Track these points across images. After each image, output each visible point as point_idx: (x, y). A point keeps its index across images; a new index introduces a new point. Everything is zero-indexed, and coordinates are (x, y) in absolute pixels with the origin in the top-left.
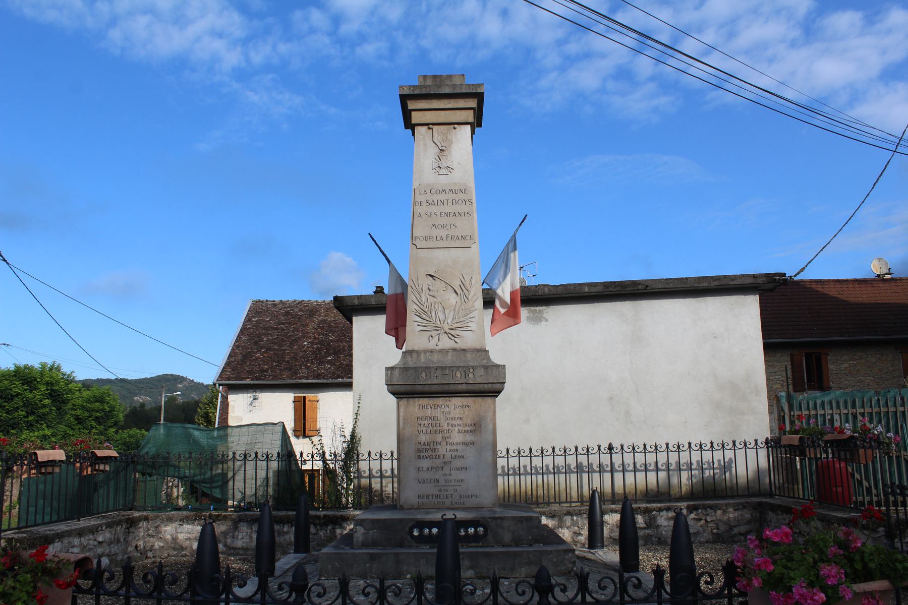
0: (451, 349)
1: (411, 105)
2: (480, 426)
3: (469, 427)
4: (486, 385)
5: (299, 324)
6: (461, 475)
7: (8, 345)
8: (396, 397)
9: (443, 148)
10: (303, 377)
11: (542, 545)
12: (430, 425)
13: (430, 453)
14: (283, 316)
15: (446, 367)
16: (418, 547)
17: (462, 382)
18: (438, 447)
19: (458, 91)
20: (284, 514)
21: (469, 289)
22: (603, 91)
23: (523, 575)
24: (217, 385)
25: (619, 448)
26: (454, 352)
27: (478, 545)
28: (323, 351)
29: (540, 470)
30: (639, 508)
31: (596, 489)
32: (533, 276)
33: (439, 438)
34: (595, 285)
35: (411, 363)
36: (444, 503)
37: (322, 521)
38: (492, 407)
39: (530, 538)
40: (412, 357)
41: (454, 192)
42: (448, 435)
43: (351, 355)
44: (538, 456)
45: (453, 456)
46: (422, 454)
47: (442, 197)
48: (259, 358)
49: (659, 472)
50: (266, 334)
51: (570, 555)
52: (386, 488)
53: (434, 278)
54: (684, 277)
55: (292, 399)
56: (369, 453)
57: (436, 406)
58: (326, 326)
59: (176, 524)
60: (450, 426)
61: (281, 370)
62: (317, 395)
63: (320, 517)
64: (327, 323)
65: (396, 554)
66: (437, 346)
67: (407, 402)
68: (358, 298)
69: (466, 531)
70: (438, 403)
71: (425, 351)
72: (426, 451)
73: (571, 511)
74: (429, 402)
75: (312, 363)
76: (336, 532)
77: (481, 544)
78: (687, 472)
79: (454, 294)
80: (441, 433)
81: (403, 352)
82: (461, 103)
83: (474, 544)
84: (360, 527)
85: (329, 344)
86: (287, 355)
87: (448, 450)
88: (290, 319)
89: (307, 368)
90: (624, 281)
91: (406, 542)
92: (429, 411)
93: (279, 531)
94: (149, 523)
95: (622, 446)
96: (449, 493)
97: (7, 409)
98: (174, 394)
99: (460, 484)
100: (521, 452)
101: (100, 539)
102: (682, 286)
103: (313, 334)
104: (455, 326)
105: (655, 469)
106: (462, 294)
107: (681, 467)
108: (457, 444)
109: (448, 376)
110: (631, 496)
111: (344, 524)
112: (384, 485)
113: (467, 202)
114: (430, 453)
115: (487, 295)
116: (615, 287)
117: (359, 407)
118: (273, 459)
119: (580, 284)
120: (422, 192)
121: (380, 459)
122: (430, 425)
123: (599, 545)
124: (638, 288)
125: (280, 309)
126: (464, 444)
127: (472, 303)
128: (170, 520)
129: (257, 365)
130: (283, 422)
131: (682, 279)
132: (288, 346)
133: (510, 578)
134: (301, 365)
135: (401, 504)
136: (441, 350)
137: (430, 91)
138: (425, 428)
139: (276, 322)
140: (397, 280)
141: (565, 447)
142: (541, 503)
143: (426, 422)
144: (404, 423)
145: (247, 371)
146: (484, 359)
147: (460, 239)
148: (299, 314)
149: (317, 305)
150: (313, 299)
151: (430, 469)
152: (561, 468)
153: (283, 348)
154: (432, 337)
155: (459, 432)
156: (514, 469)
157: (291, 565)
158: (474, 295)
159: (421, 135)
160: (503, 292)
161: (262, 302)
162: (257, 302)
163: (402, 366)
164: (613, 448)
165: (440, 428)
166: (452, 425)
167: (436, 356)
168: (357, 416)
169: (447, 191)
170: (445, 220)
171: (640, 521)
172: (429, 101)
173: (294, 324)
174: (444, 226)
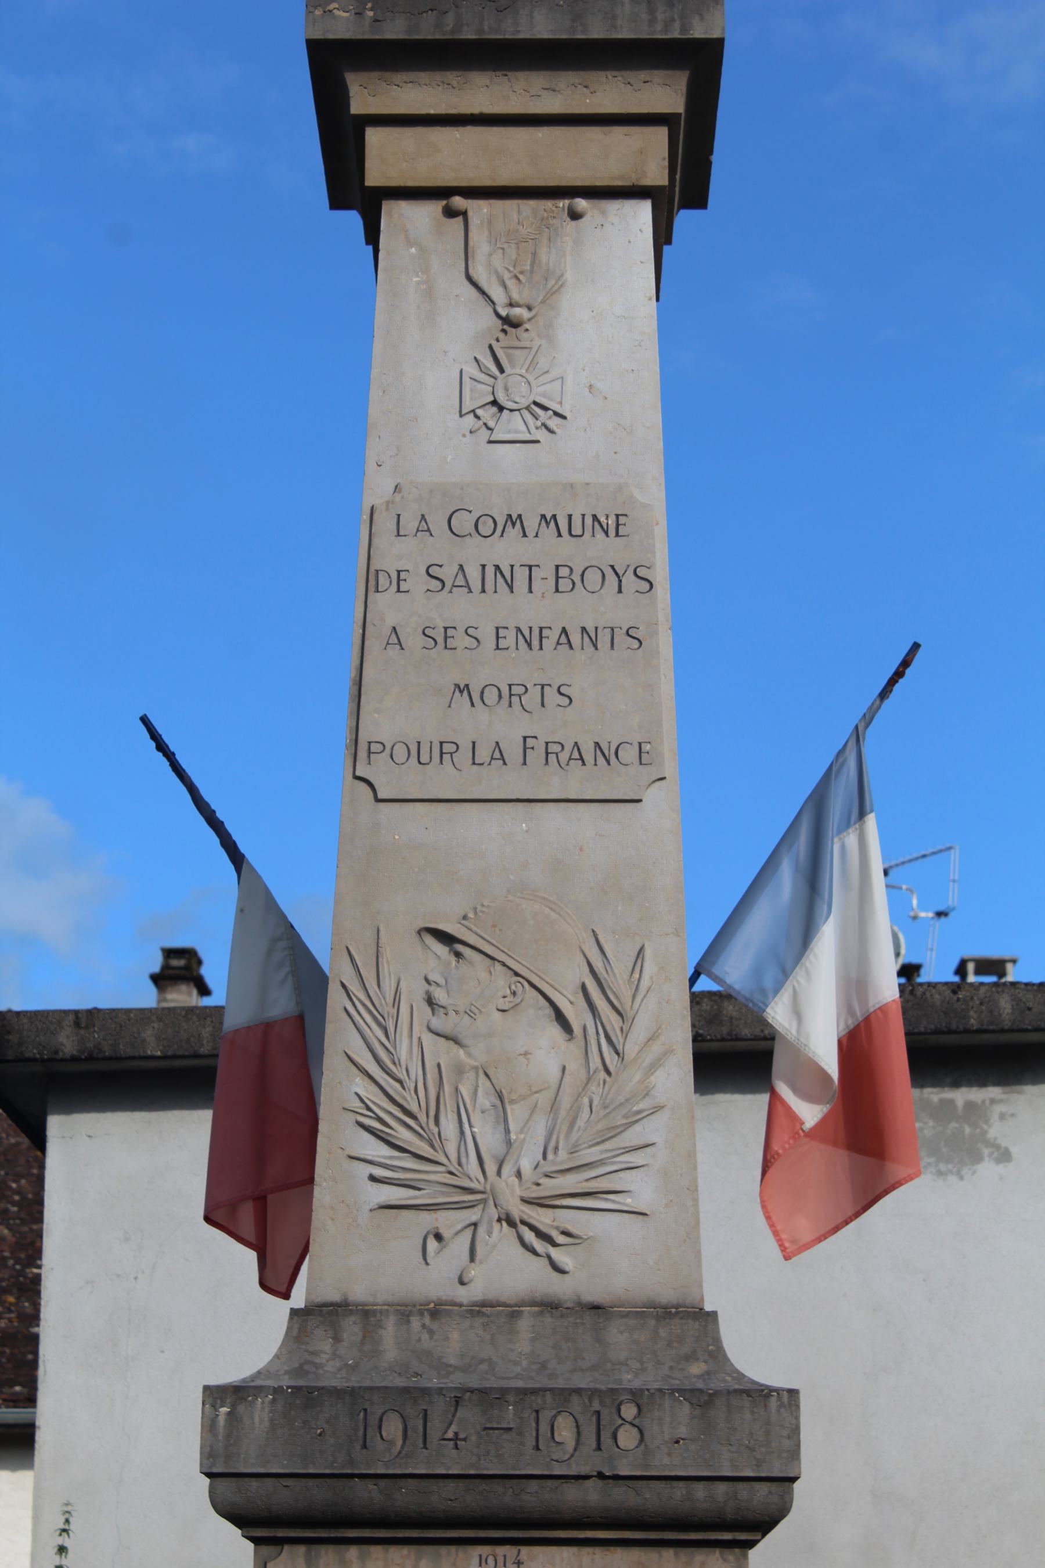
0: (533, 1303)
4: (700, 1490)
17: (584, 1470)
21: (626, 1005)
32: (940, 914)
35: (331, 1366)
40: (337, 1339)
43: (32, 1288)
53: (460, 948)
66: (462, 1283)
68: (77, 1024)
79: (555, 1031)
81: (294, 1312)
113: (629, 579)
120: (410, 524)
127: (638, 1077)
136: (484, 1304)
147: (589, 757)
154: (438, 1237)
160: (797, 1013)
163: (286, 1382)
167: (455, 1336)
172: (452, 77)
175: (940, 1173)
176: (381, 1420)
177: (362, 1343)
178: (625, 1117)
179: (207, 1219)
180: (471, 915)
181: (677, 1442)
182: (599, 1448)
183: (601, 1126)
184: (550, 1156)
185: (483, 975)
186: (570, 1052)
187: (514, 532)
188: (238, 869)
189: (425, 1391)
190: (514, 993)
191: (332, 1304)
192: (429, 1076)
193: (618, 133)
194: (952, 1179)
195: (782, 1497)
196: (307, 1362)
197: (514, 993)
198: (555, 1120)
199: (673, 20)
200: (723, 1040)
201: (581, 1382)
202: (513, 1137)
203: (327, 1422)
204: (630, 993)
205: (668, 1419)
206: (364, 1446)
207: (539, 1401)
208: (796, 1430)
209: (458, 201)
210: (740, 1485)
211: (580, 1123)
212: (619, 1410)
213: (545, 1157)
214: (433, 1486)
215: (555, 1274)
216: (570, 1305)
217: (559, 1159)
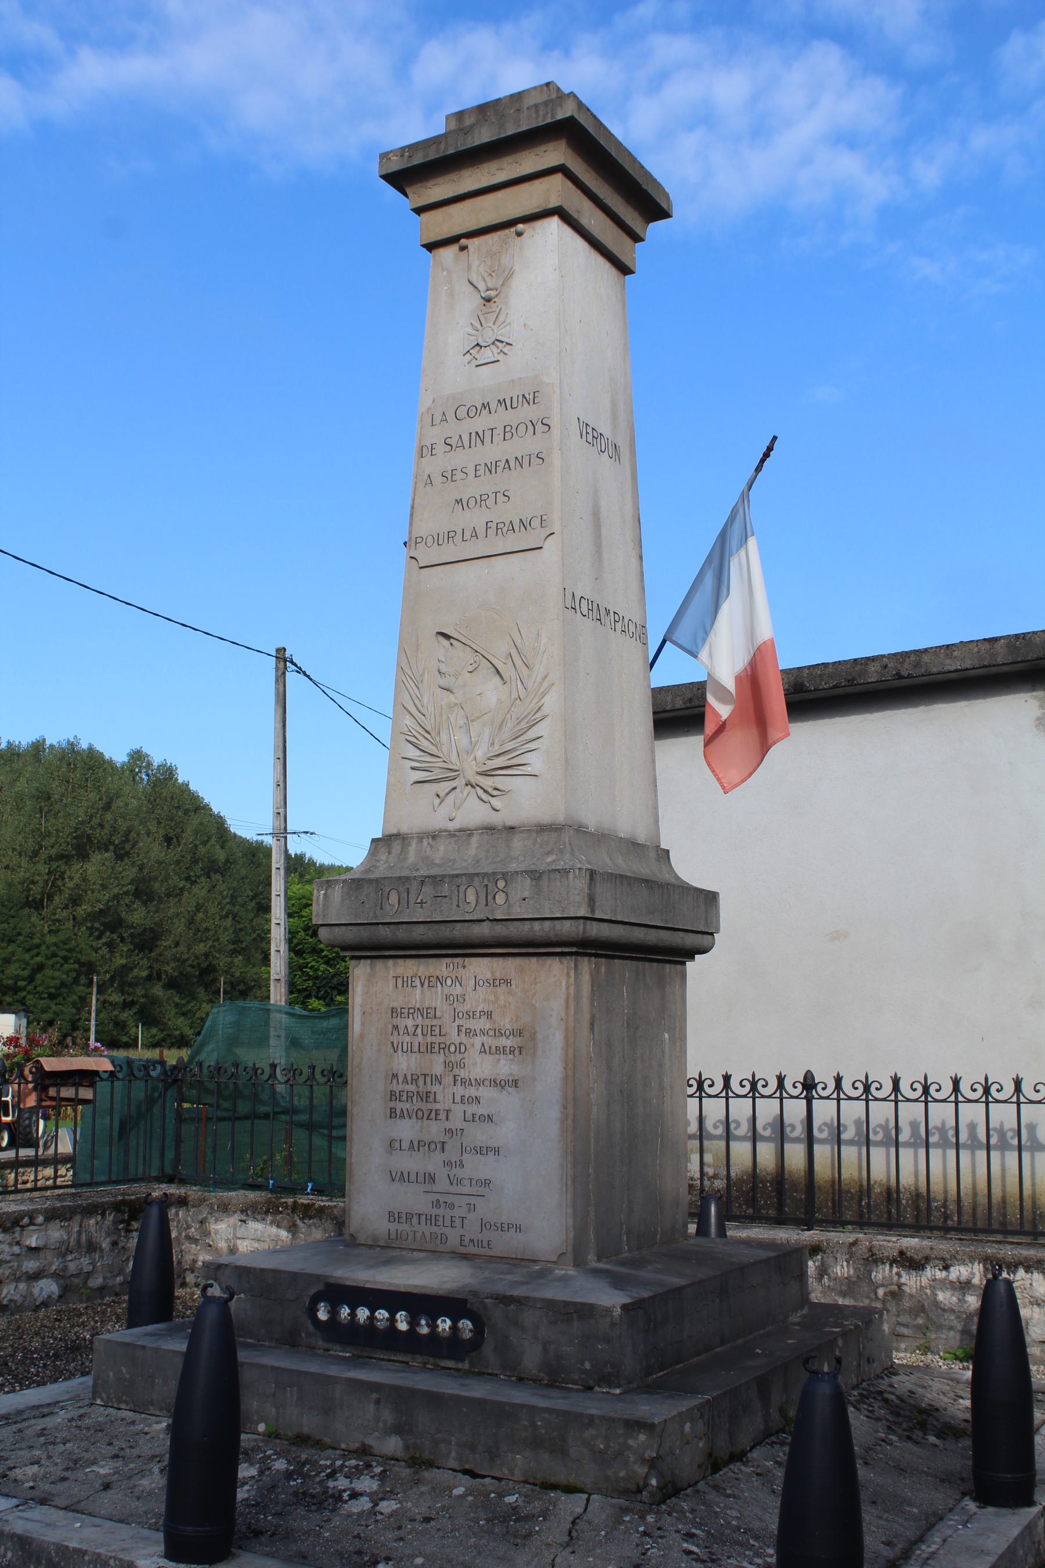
2: (533, 1036)
3: (507, 1038)
4: (537, 925)
7: (312, 834)
12: (419, 1031)
13: (418, 1104)
15: (443, 876)
16: (328, 1350)
27: (460, 1366)
29: (1012, 1138)
36: (444, 1239)
40: (390, 853)
42: (459, 1057)
45: (469, 1116)
46: (399, 1106)
47: (481, 423)
51: (642, 1437)
53: (452, 641)
59: (234, 1219)
67: (372, 968)
69: (433, 1326)
70: (439, 973)
71: (421, 837)
74: (418, 970)
79: (497, 679)
80: (442, 1051)
82: (529, 161)
83: (450, 1364)
87: (458, 1099)
91: (303, 1335)
94: (189, 1211)
96: (457, 1213)
97: (326, 956)
101: (33, 1242)
108: (479, 1083)
109: (447, 899)
113: (539, 427)
115: (915, 666)
120: (438, 418)
122: (419, 1031)
126: (495, 1083)
128: (225, 1208)
133: (483, 1477)
137: (446, 149)
138: (407, 1039)
143: (410, 1023)
144: (363, 1024)
147: (516, 528)
159: (443, 270)
166: (468, 1032)
167: (442, 848)
170: (486, 485)
172: (453, 176)
174: (481, 500)
181: (524, 900)
182: (487, 905)
187: (485, 412)
189: (408, 878)
193: (537, 183)
199: (547, 113)
200: (923, 675)
203: (366, 896)
205: (520, 888)
206: (381, 908)
209: (463, 242)
210: (557, 922)
212: (496, 884)
214: (414, 927)
216: (500, 828)
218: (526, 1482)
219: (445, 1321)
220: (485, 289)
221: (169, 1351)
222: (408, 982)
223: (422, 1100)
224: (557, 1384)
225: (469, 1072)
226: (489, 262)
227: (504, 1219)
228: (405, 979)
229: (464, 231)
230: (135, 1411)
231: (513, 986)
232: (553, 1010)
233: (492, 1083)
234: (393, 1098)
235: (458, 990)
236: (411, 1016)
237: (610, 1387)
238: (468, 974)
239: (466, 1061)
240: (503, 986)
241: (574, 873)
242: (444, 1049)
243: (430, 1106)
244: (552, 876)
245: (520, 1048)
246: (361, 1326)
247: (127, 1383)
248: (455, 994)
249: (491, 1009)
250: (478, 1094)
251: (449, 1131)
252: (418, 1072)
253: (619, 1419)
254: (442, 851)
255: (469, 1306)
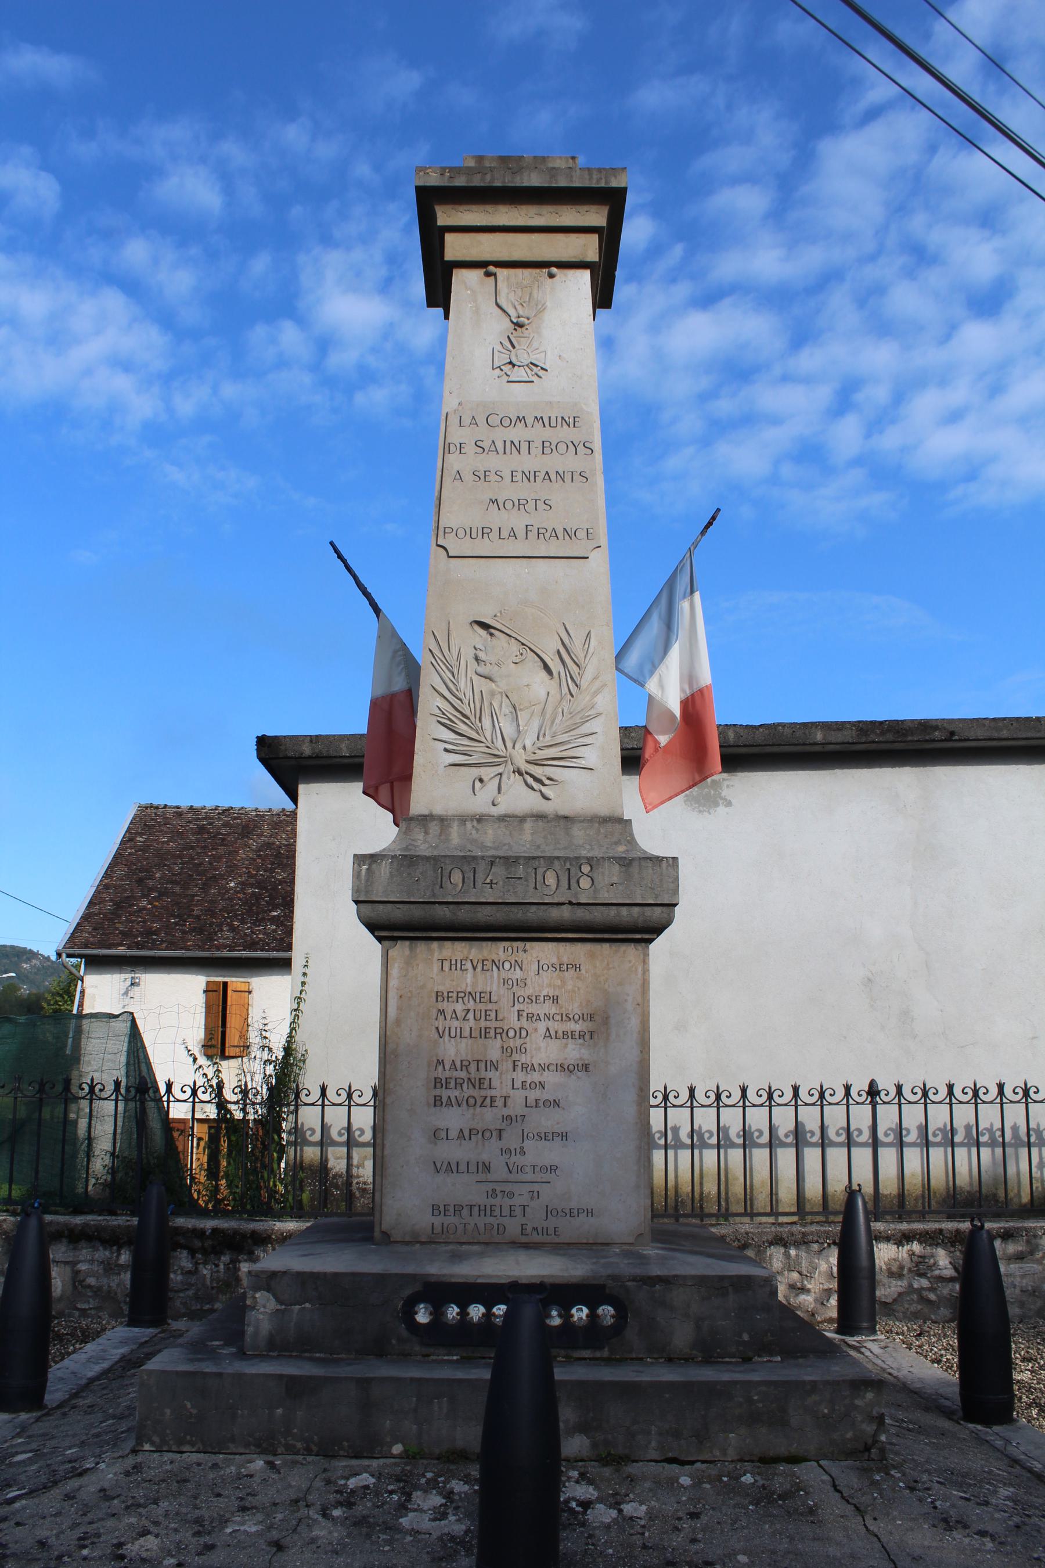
0: (532, 816)
1: (445, 216)
2: (606, 1021)
4: (624, 911)
5: (222, 850)
6: (551, 1153)
8: (380, 939)
9: (521, 319)
10: (225, 946)
11: (779, 1359)
12: (471, 1015)
13: (468, 1091)
14: (193, 834)
15: (517, 858)
16: (428, 1356)
18: (492, 1074)
19: (562, 182)
20: (121, 1223)
21: (581, 662)
22: (774, 480)
23: (732, 1454)
24: (64, 956)
25: (893, 1091)
26: (540, 823)
27: (598, 1354)
28: (263, 899)
29: (659, 1139)
30: (941, 1231)
31: (857, 1188)
33: (493, 1050)
34: (839, 726)
36: (501, 1229)
37: (208, 1243)
38: (640, 969)
39: (746, 1337)
40: (426, 833)
41: (547, 423)
42: (519, 1042)
44: (709, 1106)
45: (531, 1101)
46: (445, 1094)
47: (517, 434)
48: (145, 908)
49: (904, 1149)
50: (160, 866)
51: (870, 1395)
52: (361, 1169)
53: (492, 631)
54: (1034, 715)
55: (203, 986)
56: (324, 1090)
57: (488, 963)
58: (271, 855)
60: (524, 1019)
61: (184, 932)
62: (249, 980)
63: (205, 1232)
64: (274, 849)
65: (364, 1383)
66: (494, 805)
68: (311, 741)
69: (566, 1316)
71: (463, 819)
72: (459, 1084)
73: (785, 1236)
74: (469, 953)
75: (243, 921)
76: (239, 1270)
77: (606, 1353)
78: (942, 1149)
79: (543, 674)
80: (498, 1036)
82: (569, 216)
83: (586, 1353)
84: (265, 1293)
85: (275, 888)
86: (196, 906)
87: (518, 1084)
88: (205, 840)
89: (233, 929)
90: (903, 721)
91: (394, 1342)
92: (469, 975)
93: (109, 1264)
95: (899, 1088)
96: (517, 1201)
98: (4, 976)
99: (546, 1177)
100: (671, 1097)
102: (1029, 735)
103: (246, 868)
104: (541, 754)
105: (870, 1141)
106: (563, 674)
107: (931, 1138)
108: (543, 1068)
109: (523, 880)
110: (913, 1203)
111: (259, 1252)
112: (355, 1162)
113: (580, 448)
114: (468, 1091)
116: (883, 733)
117: (303, 983)
118: (104, 1095)
119: (805, 725)
120: (467, 420)
121: (346, 1103)
122: (471, 1015)
123: (865, 1325)
124: (932, 737)
125: (189, 822)
126: (562, 1068)
127: (588, 698)
129: (140, 922)
130: (132, 1014)
131: (1028, 719)
132: (200, 888)
133: (692, 1463)
134: (220, 925)
135: (384, 1227)
136: (506, 816)
137: (493, 179)
138: (455, 1024)
139: (179, 844)
140: (393, 657)
141: (770, 1088)
142: (711, 1215)
143: (459, 1007)
144: (399, 1008)
145: (121, 932)
146: (618, 843)
147: (560, 536)
148: (223, 831)
149: (257, 816)
150: (250, 805)
151: (466, 1134)
152: (707, 1135)
153: (190, 892)
154: (481, 780)
155: (548, 1034)
156: (990, 1130)
157: (106, 1365)
158: (595, 678)
160: (661, 686)
161: (157, 808)
162: (146, 808)
163: (398, 853)
164: (878, 1093)
165: (498, 1024)
166: (530, 1017)
167: (490, 831)
168: (298, 1003)
169: (530, 421)
170: (523, 490)
171: (941, 1263)
172: (489, 208)
173: (213, 849)
174: (520, 504)
175: (700, 811)
176: (450, 873)
177: (440, 835)
178: (581, 718)
179: (364, 793)
180: (498, 615)
182: (569, 888)
183: (568, 723)
184: (541, 738)
185: (505, 645)
186: (552, 685)
187: (521, 425)
188: (378, 617)
189: (474, 858)
190: (522, 654)
191: (424, 816)
192: (476, 697)
194: (706, 814)
195: (669, 914)
196: (410, 844)
197: (522, 654)
198: (544, 720)
201: (557, 854)
202: (521, 728)
203: (421, 874)
204: (583, 655)
205: (607, 873)
206: (441, 887)
207: (537, 863)
208: (677, 879)
210: (646, 908)
211: (557, 721)
213: (538, 739)
214: (479, 908)
215: (544, 800)
217: (546, 740)
218: (742, 1460)
219: (581, 1310)
220: (516, 315)
221: (258, 1375)
222: (458, 965)
223: (474, 1087)
224: (713, 1359)
225: (532, 1057)
226: (519, 292)
227: (573, 1205)
228: (453, 962)
229: (495, 259)
230: (205, 1453)
231: (583, 971)
232: (628, 995)
233: (559, 1067)
234: (438, 1085)
235: (518, 974)
236: (460, 1000)
237: (771, 1355)
238: (529, 958)
239: (528, 1046)
240: (572, 971)
241: (667, 862)
242: (501, 1034)
243: (483, 1093)
244: (643, 863)
245: (591, 1033)
246: (474, 1324)
247: (193, 1420)
248: (514, 978)
249: (556, 993)
250: (542, 1080)
251: (509, 1118)
252: (469, 1058)
253: (844, 1381)
254: (490, 837)
255: (607, 1291)
